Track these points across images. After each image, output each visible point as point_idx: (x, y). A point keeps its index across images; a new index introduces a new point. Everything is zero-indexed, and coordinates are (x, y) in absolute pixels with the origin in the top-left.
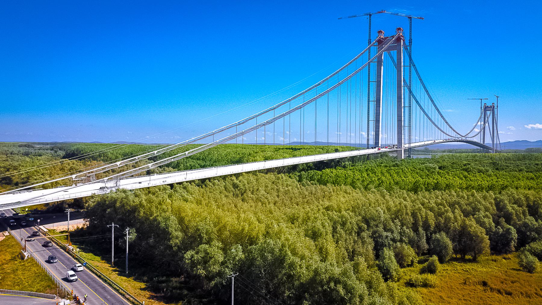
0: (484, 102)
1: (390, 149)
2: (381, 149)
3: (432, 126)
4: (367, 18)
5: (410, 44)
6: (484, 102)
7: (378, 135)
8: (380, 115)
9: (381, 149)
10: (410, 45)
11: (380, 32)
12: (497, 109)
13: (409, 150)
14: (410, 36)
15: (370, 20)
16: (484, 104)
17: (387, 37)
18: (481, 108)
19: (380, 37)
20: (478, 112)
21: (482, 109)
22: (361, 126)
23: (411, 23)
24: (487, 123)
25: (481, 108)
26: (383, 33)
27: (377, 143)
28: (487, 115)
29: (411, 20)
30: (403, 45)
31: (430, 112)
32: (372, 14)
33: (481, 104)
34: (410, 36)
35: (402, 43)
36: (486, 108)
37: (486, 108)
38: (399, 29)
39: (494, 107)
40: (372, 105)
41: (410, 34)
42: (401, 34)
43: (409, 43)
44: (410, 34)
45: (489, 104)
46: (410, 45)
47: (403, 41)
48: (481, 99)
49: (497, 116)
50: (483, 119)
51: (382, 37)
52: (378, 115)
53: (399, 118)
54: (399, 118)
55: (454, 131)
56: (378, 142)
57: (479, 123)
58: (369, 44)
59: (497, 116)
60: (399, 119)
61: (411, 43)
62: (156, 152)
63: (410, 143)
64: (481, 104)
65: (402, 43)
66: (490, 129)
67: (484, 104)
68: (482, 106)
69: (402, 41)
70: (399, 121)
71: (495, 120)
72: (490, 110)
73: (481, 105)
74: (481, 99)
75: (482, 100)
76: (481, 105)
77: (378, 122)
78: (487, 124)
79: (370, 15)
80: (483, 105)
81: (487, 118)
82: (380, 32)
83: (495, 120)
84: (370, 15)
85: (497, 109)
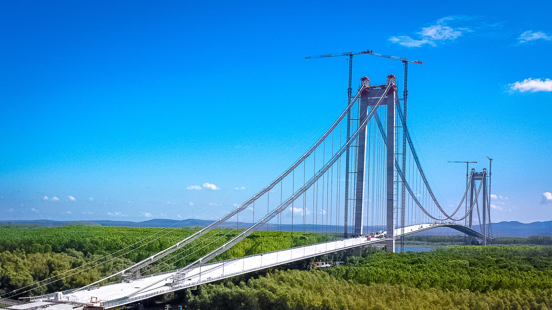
0: (471, 166)
1: (380, 239)
2: (371, 239)
3: (430, 208)
5: (404, 97)
6: (471, 166)
7: (360, 219)
8: (362, 192)
10: (404, 98)
11: (364, 79)
12: (490, 178)
13: (402, 239)
14: (406, 86)
17: (374, 87)
18: (467, 175)
20: (462, 183)
21: (469, 177)
22: (338, 206)
23: (406, 68)
24: (476, 204)
27: (358, 230)
28: (475, 190)
29: (406, 65)
31: (415, 189)
32: (354, 54)
33: (468, 170)
34: (406, 86)
35: (395, 96)
36: (475, 176)
37: (475, 176)
38: (391, 77)
39: (485, 174)
43: (404, 95)
45: (479, 170)
46: (405, 98)
47: (396, 92)
48: (468, 163)
49: (490, 188)
50: (469, 198)
51: (367, 86)
52: (360, 192)
56: (359, 228)
59: (490, 188)
60: (389, 198)
61: (407, 95)
64: (468, 170)
65: (395, 96)
66: (479, 214)
68: (469, 173)
69: (395, 92)
70: (390, 200)
71: (487, 201)
73: (467, 171)
75: (468, 164)
76: (467, 171)
77: (360, 202)
78: (475, 206)
79: (351, 55)
80: (470, 171)
81: (476, 195)
82: (364, 79)
83: (487, 201)
84: (351, 55)
85: (490, 178)
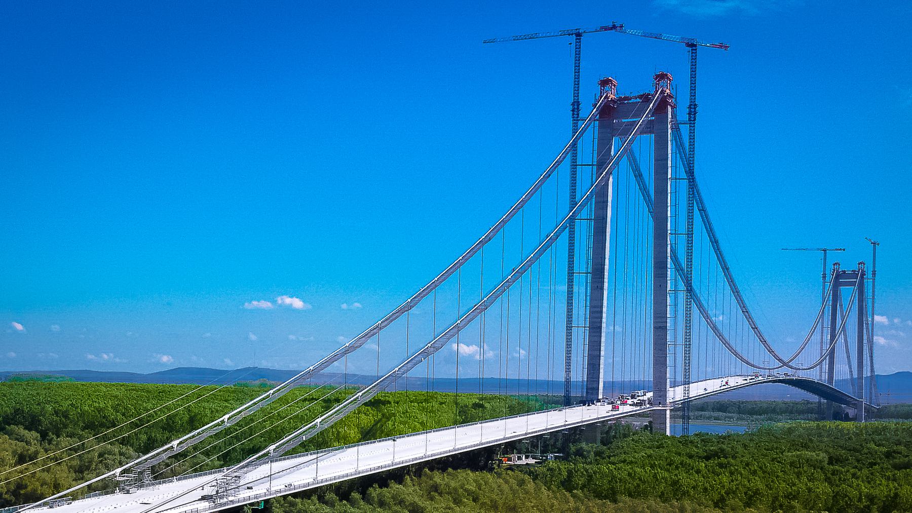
0: (832, 258)
2: (621, 408)
4: (571, 44)
6: (832, 258)
9: (621, 408)
10: (690, 120)
11: (605, 83)
12: (874, 282)
14: (693, 95)
15: (578, 48)
16: (859, 264)
17: (626, 98)
18: (824, 277)
19: (606, 97)
23: (694, 59)
25: (824, 277)
26: (614, 86)
30: (671, 121)
34: (693, 95)
35: (670, 116)
36: (840, 278)
37: (840, 278)
38: (662, 77)
39: (863, 275)
40: (581, 290)
41: (693, 89)
42: (668, 91)
43: (689, 114)
44: (693, 89)
45: (848, 266)
47: (673, 108)
48: (825, 250)
51: (612, 96)
53: (659, 322)
54: (659, 322)
55: (771, 351)
57: (816, 337)
58: (573, 114)
62: (175, 443)
63: (687, 382)
65: (670, 116)
67: (834, 265)
68: (828, 272)
72: (853, 284)
74: (825, 250)
75: (825, 254)
78: (841, 340)
79: (579, 35)
80: (830, 267)
82: (605, 83)
83: (867, 328)
84: (579, 35)
